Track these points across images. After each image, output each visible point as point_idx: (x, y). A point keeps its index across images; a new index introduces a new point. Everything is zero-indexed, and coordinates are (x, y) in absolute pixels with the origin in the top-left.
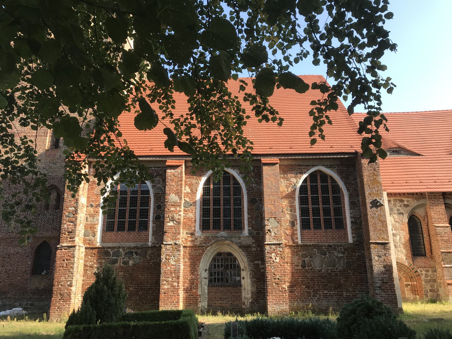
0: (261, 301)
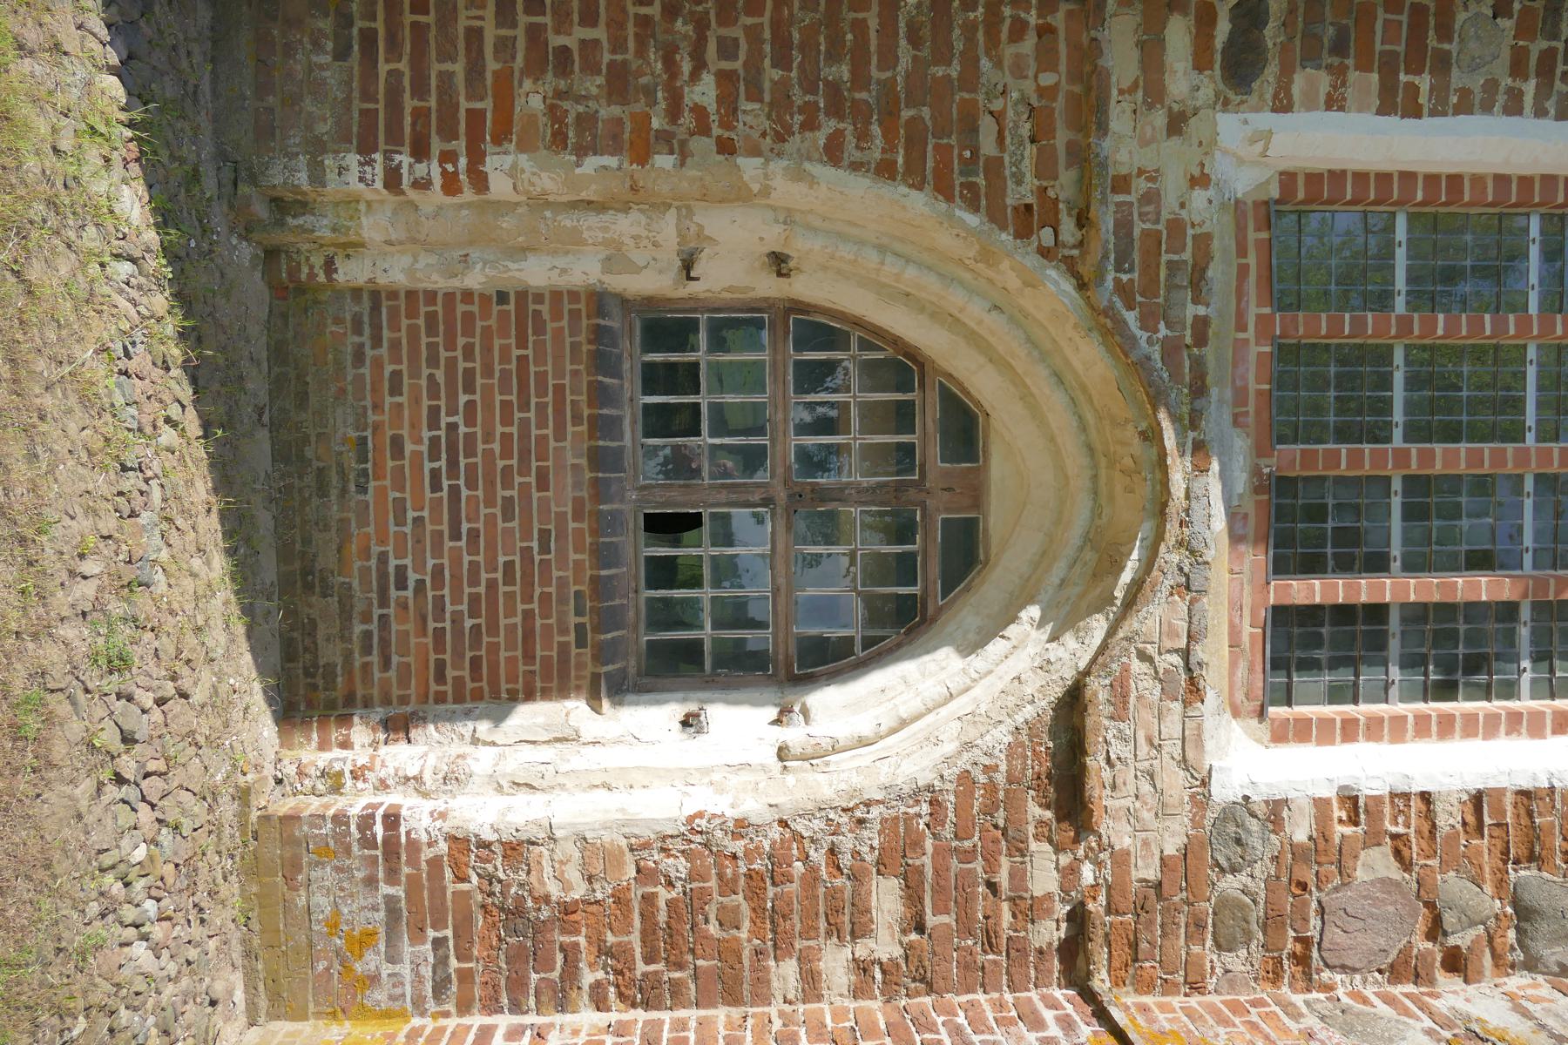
0: (416, 956)
